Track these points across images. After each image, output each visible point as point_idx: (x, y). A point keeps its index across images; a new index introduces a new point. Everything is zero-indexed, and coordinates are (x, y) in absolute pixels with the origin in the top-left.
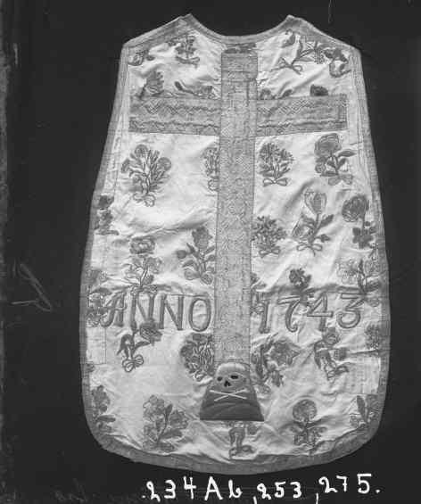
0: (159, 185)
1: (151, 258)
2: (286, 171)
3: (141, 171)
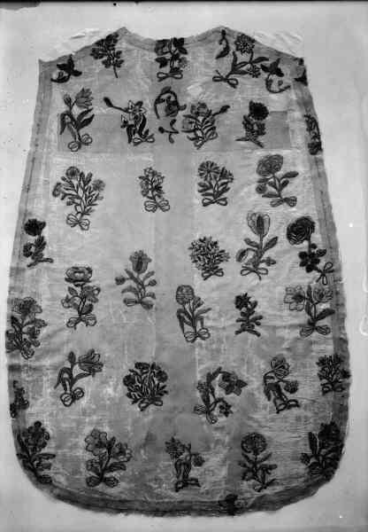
0: (93, 208)
1: (89, 287)
2: (226, 190)
3: (74, 193)
